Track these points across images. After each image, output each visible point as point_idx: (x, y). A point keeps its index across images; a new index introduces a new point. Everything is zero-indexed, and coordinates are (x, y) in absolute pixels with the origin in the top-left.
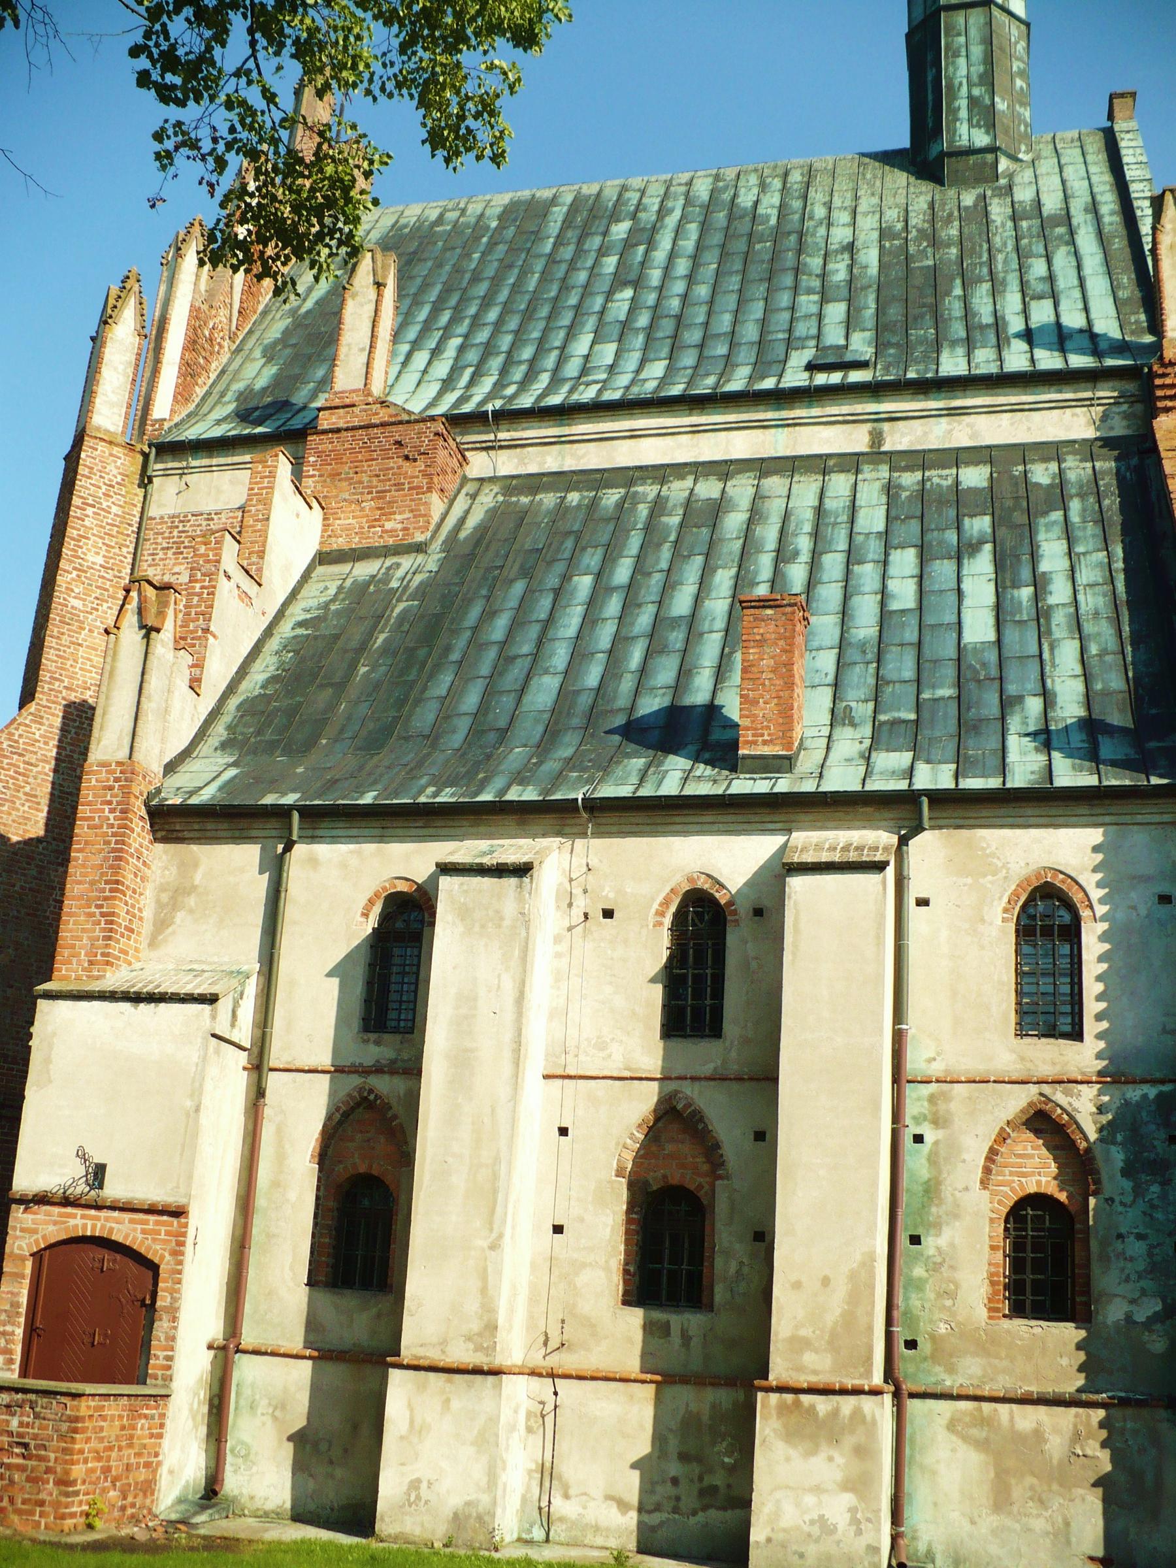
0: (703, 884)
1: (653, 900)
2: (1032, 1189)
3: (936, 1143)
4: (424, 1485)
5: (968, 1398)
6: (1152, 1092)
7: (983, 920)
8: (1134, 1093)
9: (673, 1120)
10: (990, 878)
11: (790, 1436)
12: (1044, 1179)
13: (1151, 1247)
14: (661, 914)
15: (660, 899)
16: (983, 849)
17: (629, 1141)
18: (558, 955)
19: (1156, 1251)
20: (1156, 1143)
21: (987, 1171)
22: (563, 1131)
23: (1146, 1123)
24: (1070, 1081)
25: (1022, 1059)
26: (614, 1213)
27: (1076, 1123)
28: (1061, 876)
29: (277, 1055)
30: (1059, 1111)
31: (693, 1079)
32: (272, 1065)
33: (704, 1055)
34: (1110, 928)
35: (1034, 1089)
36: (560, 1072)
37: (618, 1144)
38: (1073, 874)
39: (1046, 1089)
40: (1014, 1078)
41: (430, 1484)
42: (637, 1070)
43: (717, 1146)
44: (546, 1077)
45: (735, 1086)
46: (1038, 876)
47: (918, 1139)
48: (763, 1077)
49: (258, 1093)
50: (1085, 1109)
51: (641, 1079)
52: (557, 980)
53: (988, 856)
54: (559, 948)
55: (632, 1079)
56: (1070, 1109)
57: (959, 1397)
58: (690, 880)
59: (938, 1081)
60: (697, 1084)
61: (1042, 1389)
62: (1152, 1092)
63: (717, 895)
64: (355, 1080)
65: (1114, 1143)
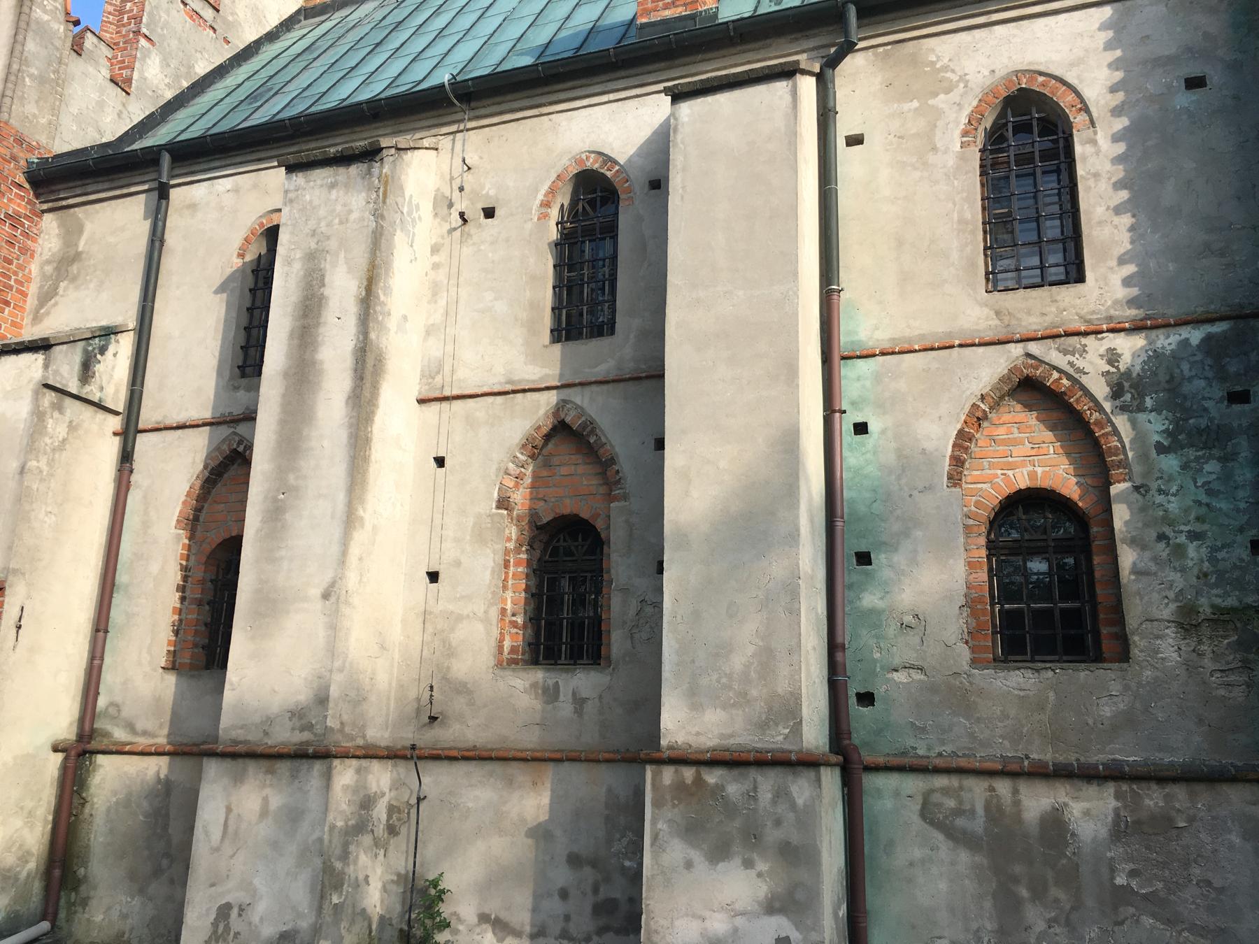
0: (593, 163)
1: (537, 191)
2: (1023, 483)
3: (883, 432)
4: (234, 913)
5: (947, 771)
6: (1195, 336)
7: (934, 149)
8: (1167, 341)
9: (565, 436)
10: (942, 96)
11: (691, 831)
12: (1039, 470)
13: (1214, 549)
14: (546, 204)
15: (545, 188)
16: (933, 63)
17: (511, 466)
18: (436, 266)
19: (1220, 555)
20: (1208, 404)
21: (957, 462)
22: (440, 462)
23: (1190, 379)
24: (1068, 334)
25: (998, 313)
26: (494, 552)
27: (1083, 388)
28: (1041, 79)
29: (147, 416)
30: (1056, 375)
31: (582, 384)
32: (141, 426)
33: (601, 356)
34: (1132, 122)
35: (1016, 350)
36: (437, 394)
37: (499, 469)
38: (1057, 73)
39: (1033, 348)
40: (987, 339)
41: (241, 909)
42: (520, 381)
43: (612, 461)
44: (421, 401)
45: (631, 387)
46: (1007, 79)
47: (861, 428)
48: (649, 377)
49: (126, 457)
50: (1092, 367)
51: (524, 391)
52: (435, 294)
53: (939, 70)
54: (436, 259)
55: (514, 392)
56: (1071, 371)
57: (937, 771)
58: (579, 161)
59: (883, 354)
60: (587, 390)
61: (1061, 759)
62: (1195, 336)
63: (609, 174)
64: (224, 431)
65: (1141, 409)
